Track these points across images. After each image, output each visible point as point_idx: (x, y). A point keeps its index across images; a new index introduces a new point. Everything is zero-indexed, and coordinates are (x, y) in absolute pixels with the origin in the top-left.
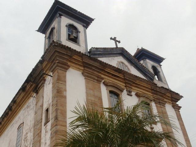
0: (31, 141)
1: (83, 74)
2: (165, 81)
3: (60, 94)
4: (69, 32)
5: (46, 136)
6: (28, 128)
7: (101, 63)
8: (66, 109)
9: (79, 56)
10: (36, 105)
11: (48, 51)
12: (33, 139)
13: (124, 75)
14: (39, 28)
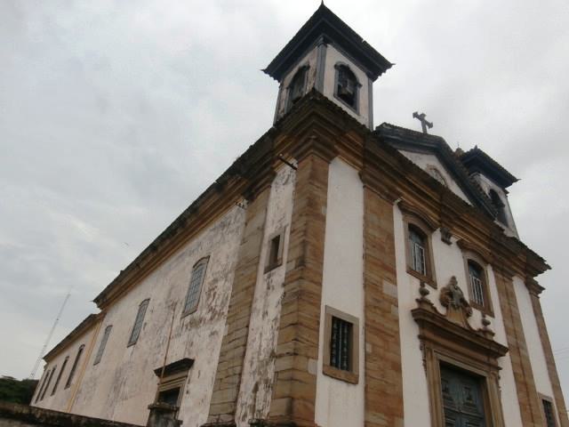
0: (227, 299)
1: (360, 175)
2: (514, 226)
3: (311, 209)
4: (339, 81)
5: (269, 298)
6: (220, 269)
7: (403, 160)
8: (323, 246)
10: (246, 224)
11: (296, 111)
12: (232, 296)
14: (269, 66)
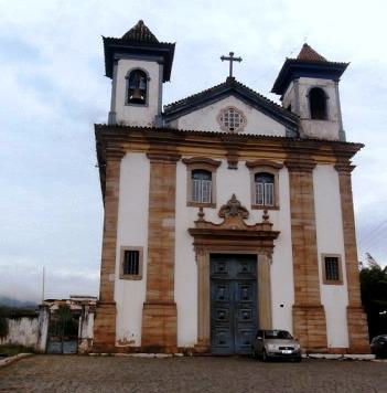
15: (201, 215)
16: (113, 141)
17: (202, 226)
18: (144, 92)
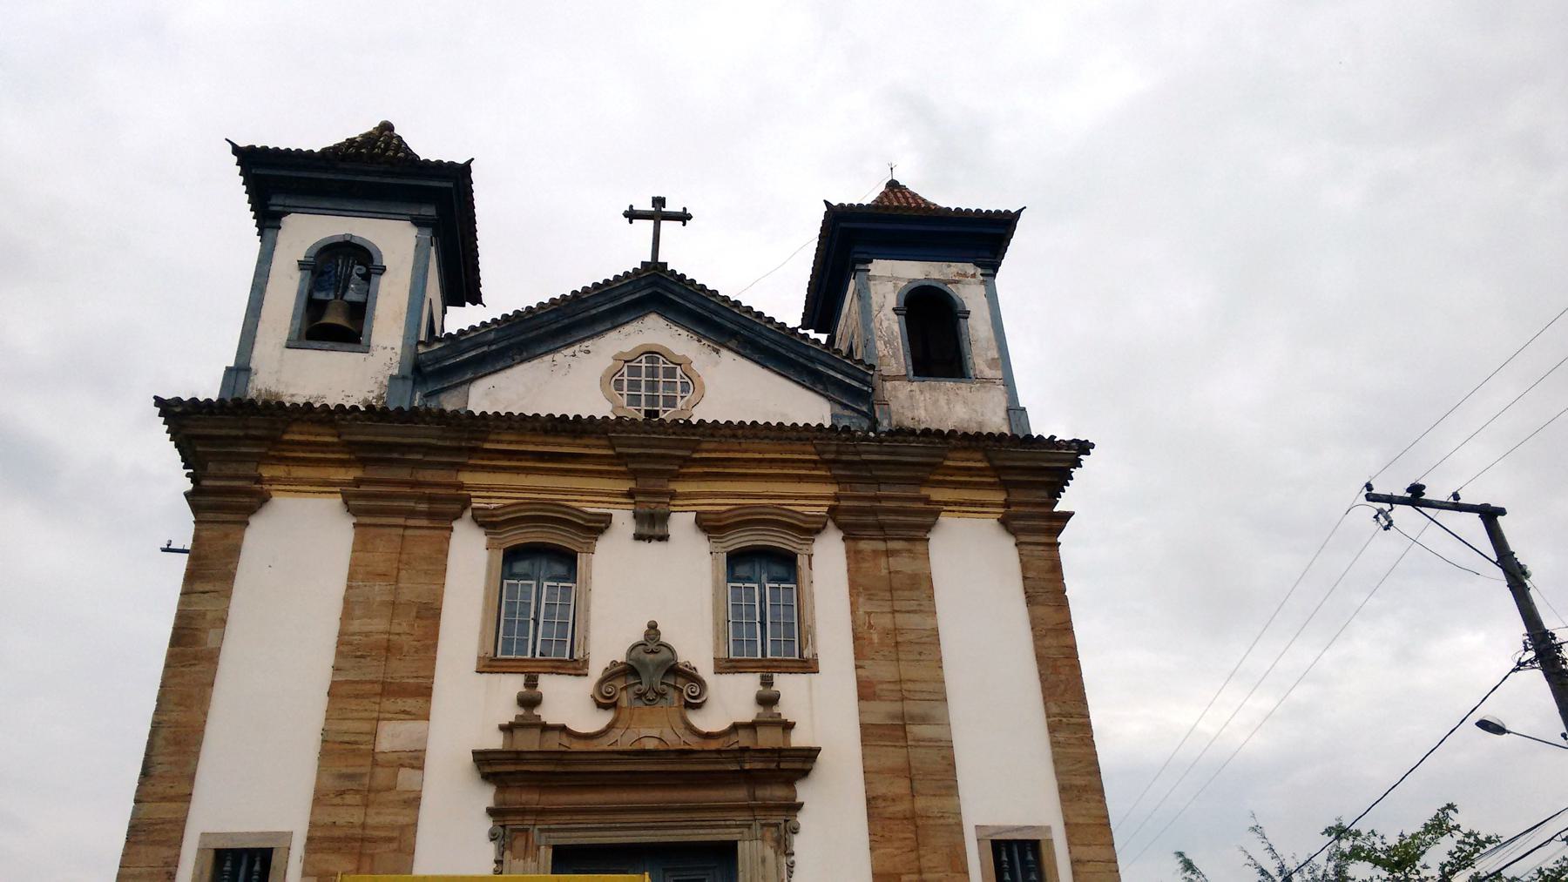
9: (320, 422)
13: (610, 439)
15: (529, 701)
16: (229, 457)
17: (528, 741)
18: (360, 311)
